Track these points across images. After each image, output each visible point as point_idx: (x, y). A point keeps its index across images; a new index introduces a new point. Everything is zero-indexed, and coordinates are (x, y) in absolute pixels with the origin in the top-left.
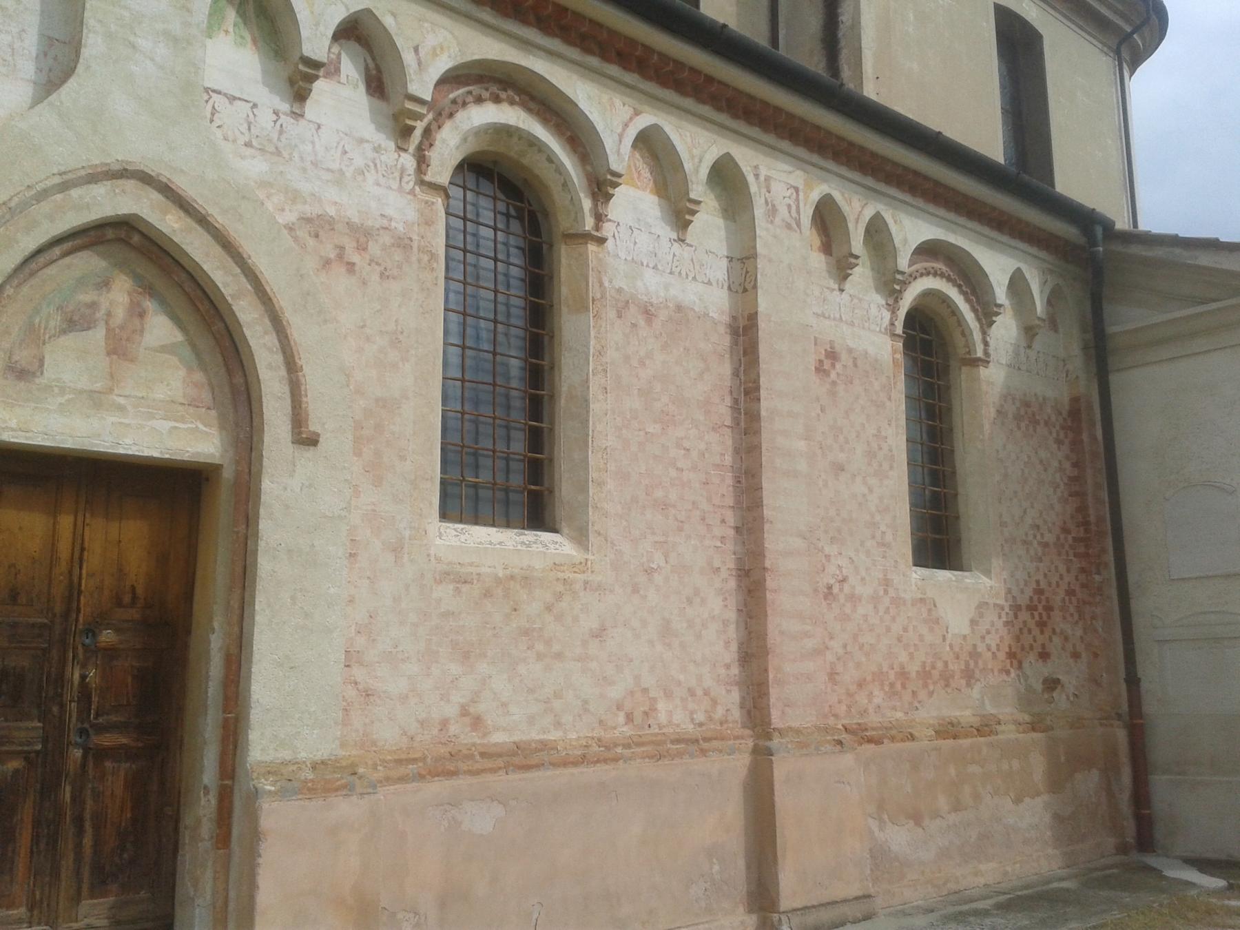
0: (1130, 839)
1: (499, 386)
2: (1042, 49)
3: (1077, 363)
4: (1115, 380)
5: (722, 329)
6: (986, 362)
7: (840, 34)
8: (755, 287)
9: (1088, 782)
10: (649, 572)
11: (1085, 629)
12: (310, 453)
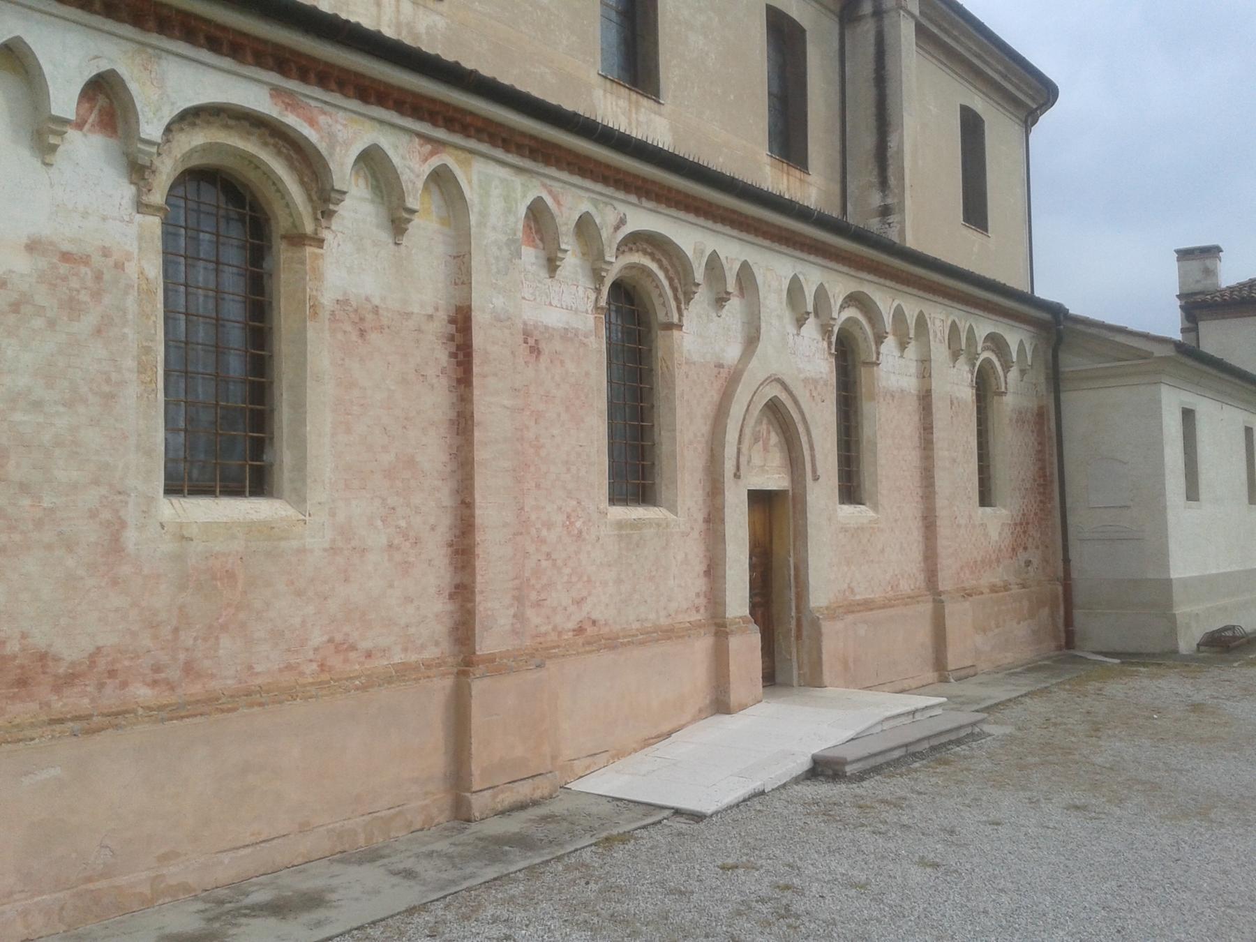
0: (1063, 643)
1: (181, 256)
2: (983, 131)
3: (1043, 388)
4: (1064, 397)
5: (915, 398)
6: (1004, 393)
7: (888, 155)
8: (930, 376)
9: (1045, 612)
10: (896, 521)
11: (1041, 534)
12: (820, 480)
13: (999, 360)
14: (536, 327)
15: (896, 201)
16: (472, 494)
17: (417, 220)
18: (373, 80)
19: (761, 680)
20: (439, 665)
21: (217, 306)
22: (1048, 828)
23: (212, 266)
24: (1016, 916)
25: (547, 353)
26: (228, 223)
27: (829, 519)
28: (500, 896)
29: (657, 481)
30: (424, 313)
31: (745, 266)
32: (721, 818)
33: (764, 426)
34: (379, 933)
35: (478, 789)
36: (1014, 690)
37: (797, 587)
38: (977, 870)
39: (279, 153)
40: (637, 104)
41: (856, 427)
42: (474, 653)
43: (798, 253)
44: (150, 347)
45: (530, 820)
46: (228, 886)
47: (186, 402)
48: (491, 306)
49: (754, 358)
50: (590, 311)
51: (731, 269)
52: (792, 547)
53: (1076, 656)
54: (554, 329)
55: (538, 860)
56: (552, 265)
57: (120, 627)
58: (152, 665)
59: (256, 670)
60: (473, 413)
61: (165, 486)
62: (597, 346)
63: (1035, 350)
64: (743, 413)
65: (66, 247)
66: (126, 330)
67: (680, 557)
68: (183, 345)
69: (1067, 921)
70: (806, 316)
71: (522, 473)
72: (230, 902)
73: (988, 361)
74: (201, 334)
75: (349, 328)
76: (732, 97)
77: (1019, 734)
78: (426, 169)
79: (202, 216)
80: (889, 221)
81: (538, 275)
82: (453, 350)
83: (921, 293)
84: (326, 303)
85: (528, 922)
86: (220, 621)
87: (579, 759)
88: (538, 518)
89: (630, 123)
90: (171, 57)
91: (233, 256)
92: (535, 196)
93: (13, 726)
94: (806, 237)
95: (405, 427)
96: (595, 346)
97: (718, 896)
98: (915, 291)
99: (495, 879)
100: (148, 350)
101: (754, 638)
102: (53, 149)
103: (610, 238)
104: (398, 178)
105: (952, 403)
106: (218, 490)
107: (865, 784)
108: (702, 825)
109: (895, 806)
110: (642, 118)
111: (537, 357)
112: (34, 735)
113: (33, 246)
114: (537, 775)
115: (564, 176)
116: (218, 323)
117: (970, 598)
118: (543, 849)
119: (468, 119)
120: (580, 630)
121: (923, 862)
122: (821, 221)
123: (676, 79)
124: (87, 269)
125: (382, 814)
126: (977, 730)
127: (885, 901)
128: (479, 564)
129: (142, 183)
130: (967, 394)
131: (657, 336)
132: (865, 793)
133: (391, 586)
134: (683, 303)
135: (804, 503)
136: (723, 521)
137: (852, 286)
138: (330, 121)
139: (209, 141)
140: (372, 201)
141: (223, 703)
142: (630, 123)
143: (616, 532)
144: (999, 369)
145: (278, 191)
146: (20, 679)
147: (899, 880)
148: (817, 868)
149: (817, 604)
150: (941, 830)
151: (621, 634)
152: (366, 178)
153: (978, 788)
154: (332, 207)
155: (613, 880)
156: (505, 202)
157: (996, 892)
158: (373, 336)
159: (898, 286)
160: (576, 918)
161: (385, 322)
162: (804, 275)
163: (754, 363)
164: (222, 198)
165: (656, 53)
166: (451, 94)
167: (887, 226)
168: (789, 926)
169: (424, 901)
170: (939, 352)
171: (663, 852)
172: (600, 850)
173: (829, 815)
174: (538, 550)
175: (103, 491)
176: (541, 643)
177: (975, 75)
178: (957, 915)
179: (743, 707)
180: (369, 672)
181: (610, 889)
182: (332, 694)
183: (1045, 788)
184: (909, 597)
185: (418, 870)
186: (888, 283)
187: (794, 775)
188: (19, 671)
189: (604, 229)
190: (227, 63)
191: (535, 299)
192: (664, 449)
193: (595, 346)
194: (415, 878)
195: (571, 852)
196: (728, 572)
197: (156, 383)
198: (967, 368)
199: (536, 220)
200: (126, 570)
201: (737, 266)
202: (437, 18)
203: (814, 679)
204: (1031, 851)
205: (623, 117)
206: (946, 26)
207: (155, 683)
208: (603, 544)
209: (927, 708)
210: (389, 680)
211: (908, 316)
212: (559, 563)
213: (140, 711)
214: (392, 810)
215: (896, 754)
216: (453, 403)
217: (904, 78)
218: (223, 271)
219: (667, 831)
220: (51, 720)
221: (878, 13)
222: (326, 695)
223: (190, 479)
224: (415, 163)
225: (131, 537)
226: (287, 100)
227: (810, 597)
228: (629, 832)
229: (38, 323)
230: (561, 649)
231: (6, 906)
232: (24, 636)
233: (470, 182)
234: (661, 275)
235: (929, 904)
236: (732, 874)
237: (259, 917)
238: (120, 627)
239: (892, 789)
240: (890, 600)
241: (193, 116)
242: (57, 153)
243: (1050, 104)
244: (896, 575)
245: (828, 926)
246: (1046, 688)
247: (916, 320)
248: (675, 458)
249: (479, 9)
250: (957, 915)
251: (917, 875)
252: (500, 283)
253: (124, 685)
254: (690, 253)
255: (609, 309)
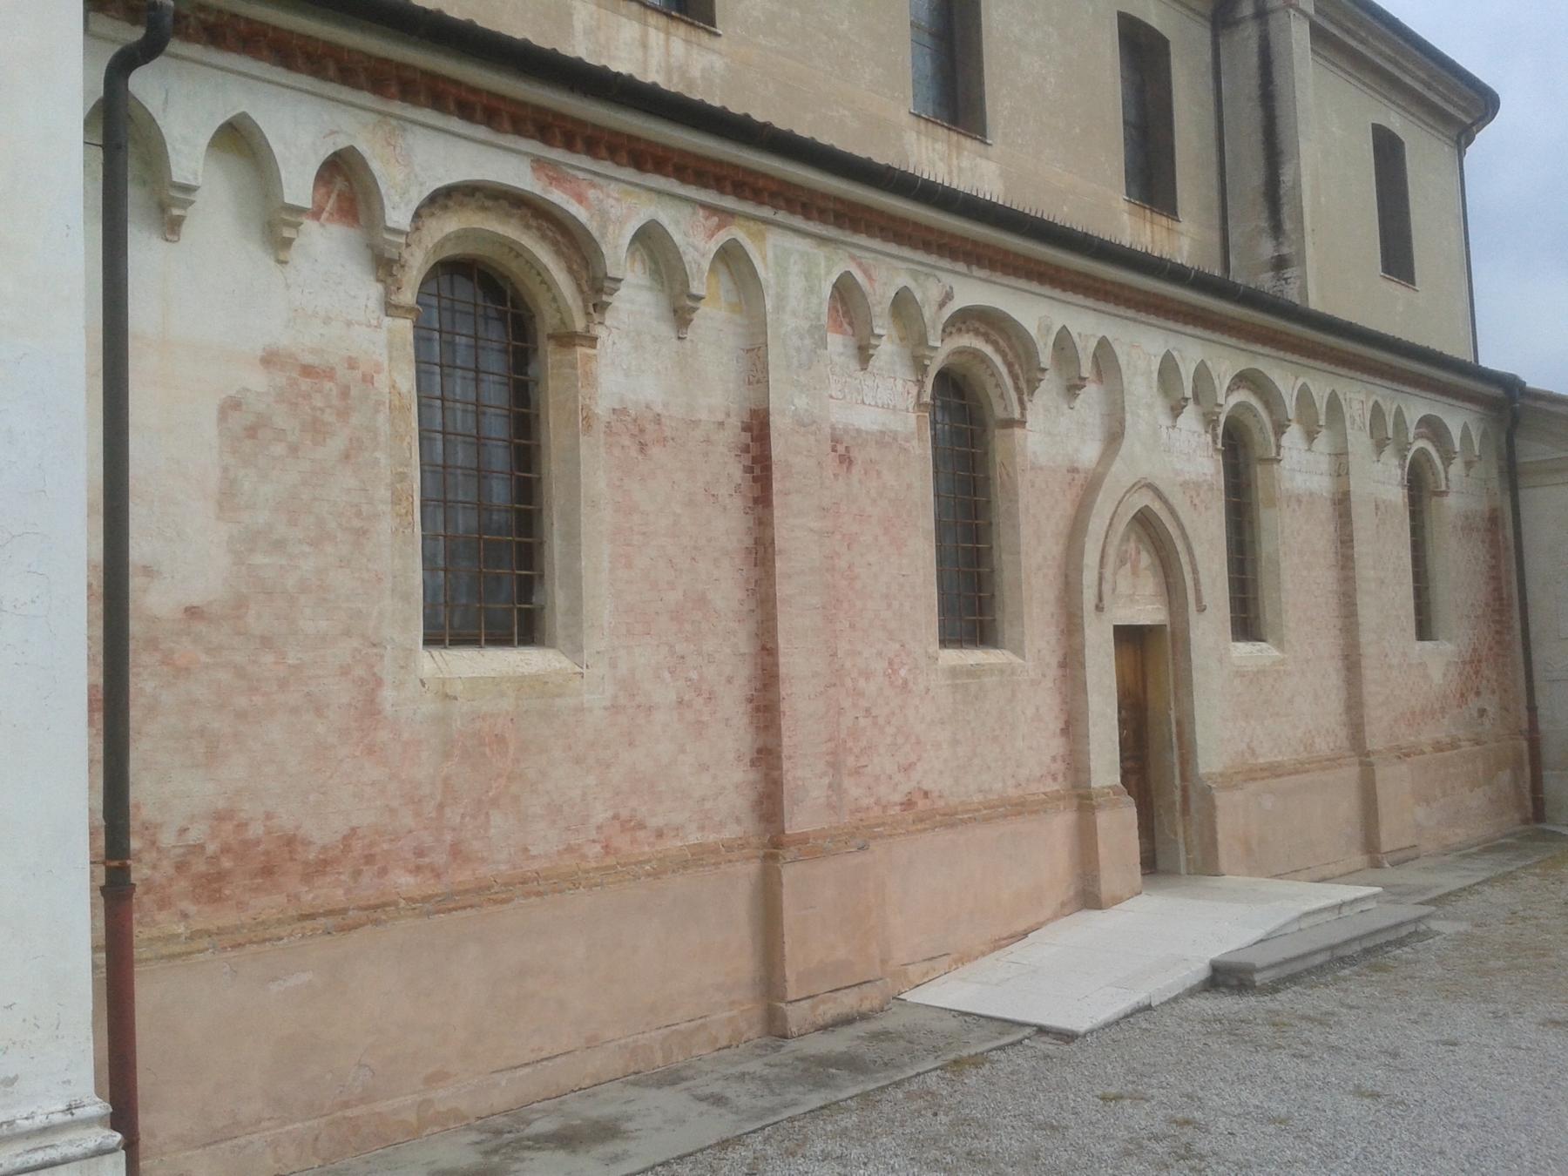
0: (1530, 815)
1: (436, 364)
2: (1404, 155)
4: (1523, 494)
5: (1328, 503)
7: (1282, 192)
8: (1347, 474)
9: (1505, 776)
10: (1307, 661)
12: (1206, 611)
13: (1438, 451)
14: (846, 431)
15: (1293, 250)
16: (774, 637)
17: (704, 309)
18: (649, 143)
19: (1139, 866)
20: (742, 847)
21: (478, 422)
22: (1519, 1048)
23: (471, 375)
24: (1482, 1159)
25: (860, 462)
26: (486, 324)
27: (1220, 661)
28: (829, 1128)
29: (997, 617)
30: (713, 420)
31: (1103, 344)
32: (1097, 1038)
33: (1132, 544)
34: (688, 1170)
35: (794, 997)
36: (1470, 876)
37: (1180, 748)
38: (1429, 1101)
39: (544, 237)
40: (959, 148)
41: (1253, 542)
42: (783, 832)
43: (1171, 324)
44: (404, 473)
45: (858, 1037)
46: (506, 1113)
47: (445, 537)
48: (793, 408)
49: (1118, 458)
50: (911, 410)
51: (1085, 348)
52: (1172, 698)
53: (1545, 831)
54: (867, 433)
55: (872, 1086)
56: (864, 354)
57: (378, 803)
58: (415, 848)
59: (532, 853)
60: (773, 540)
61: (424, 634)
62: (921, 451)
63: (1484, 435)
64: (1105, 528)
65: (309, 359)
66: (378, 454)
67: (1030, 712)
68: (441, 469)
69: (1549, 1164)
70: (1183, 404)
71: (834, 611)
72: (510, 1132)
73: (1422, 451)
74: (460, 455)
75: (626, 441)
76: (1078, 130)
77: (1477, 932)
78: (713, 247)
79: (458, 315)
80: (1286, 276)
81: (848, 368)
82: (748, 463)
83: (1331, 368)
84: (600, 412)
85: (866, 1160)
86: (490, 794)
87: (913, 963)
88: (854, 666)
89: (950, 173)
90: (417, 129)
91: (494, 362)
92: (842, 271)
93: (258, 923)
94: (1181, 303)
95: (694, 559)
96: (918, 451)
97: (1100, 1132)
98: (1325, 366)
99: (822, 1108)
100: (402, 477)
101: (1129, 813)
102: (287, 243)
103: (934, 317)
104: (681, 258)
105: (1377, 507)
106: (483, 638)
107: (1279, 996)
108: (1074, 1046)
109: (1321, 1024)
110: (965, 164)
111: (848, 468)
112: (283, 934)
113: (270, 359)
114: (865, 983)
115: (876, 244)
116: (479, 441)
117: (1408, 759)
118: (878, 1072)
119: (761, 183)
120: (908, 804)
121: (1359, 1092)
122: (1201, 282)
123: (1005, 113)
124: (332, 384)
125: (683, 1026)
126: (1422, 927)
127: (1313, 1139)
128: (785, 723)
129: (389, 280)
130: (1397, 495)
131: (994, 437)
132: (1280, 1008)
133: (683, 751)
134: (1025, 391)
135: (1187, 641)
136: (1083, 665)
137: (1243, 363)
138: (601, 196)
139: (464, 226)
140: (650, 289)
141: (496, 893)
142: (950, 173)
143: (949, 682)
144: (1438, 461)
145: (543, 282)
146: (265, 867)
147: (1330, 1113)
148: (1224, 1099)
149: (1208, 770)
150: (1381, 1052)
151: (960, 809)
152: (643, 262)
153: (1425, 1000)
154: (605, 298)
155: (967, 1111)
156: (807, 280)
157: (1456, 1129)
158: (655, 451)
159: (1304, 361)
160: (925, 1156)
161: (668, 433)
162: (1179, 351)
163: (1118, 466)
164: (480, 293)
165: (981, 84)
166: (741, 154)
167: (1283, 282)
168: (1192, 1169)
169: (738, 1133)
170: (1359, 441)
171: (1026, 1078)
172: (948, 1075)
173: (1236, 1035)
174: (855, 705)
175: (356, 643)
176: (861, 820)
177: (1387, 82)
178: (1405, 1157)
179: (1117, 900)
180: (661, 855)
181: (966, 1121)
182: (620, 881)
183: (1515, 999)
184: (1328, 760)
185: (728, 1095)
186: (1289, 356)
187: (1188, 986)
188: (263, 858)
189: (926, 307)
190: (481, 132)
191: (844, 397)
192: (1006, 576)
193: (918, 451)
194: (726, 1104)
195: (912, 1077)
196: (1092, 730)
197: (413, 515)
198: (1395, 462)
199: (843, 300)
200: (383, 735)
201: (1093, 344)
202: (714, 58)
203: (1207, 865)
204: (1498, 1078)
205: (941, 164)
206: (1350, 25)
207: (418, 869)
208: (933, 697)
209: (1356, 900)
210: (684, 865)
211: (1315, 397)
212: (881, 721)
213: (402, 903)
214: (692, 1023)
215: (1319, 959)
216: (749, 528)
217: (1298, 94)
218: (482, 380)
219: (1029, 1053)
220: (301, 915)
221: (1262, 14)
222: (612, 883)
223: (451, 627)
224: (699, 240)
225: (388, 695)
226: (551, 174)
227: (1199, 761)
228: (983, 1054)
229: (279, 449)
230: (887, 828)
231: (254, 1136)
232: (269, 816)
233: (764, 258)
234: (997, 360)
235: (1369, 1143)
236: (1116, 1106)
237: (544, 1150)
238: (378, 803)
239: (1315, 1002)
240: (1302, 763)
241: (444, 198)
242: (293, 248)
243: (1490, 117)
244: (1310, 732)
245: (1241, 1168)
246: (1511, 872)
247: (1328, 402)
248: (1020, 587)
249: (764, 42)
250: (1405, 1157)
251: (1352, 1107)
252: (803, 379)
253: (383, 872)
254: (1033, 331)
255: (934, 405)
